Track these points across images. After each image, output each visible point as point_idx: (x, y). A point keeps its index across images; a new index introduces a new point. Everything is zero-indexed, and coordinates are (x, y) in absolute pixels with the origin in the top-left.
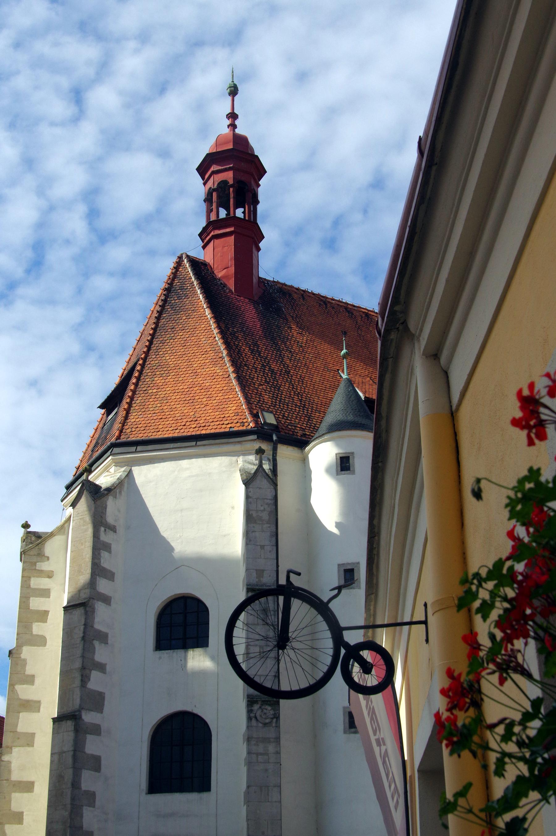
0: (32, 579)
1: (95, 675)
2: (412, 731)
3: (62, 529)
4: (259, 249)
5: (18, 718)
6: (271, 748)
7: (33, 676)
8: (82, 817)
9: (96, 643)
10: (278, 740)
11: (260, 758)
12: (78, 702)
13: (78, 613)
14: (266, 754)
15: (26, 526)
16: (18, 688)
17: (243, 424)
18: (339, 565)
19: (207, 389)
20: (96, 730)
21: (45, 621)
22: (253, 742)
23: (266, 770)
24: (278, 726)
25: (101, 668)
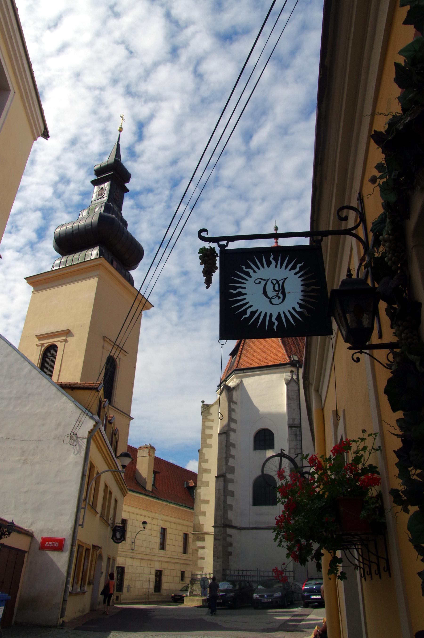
8: (228, 514)
9: (231, 448)
12: (225, 470)
15: (203, 402)
16: (202, 464)
20: (232, 481)
21: (211, 439)
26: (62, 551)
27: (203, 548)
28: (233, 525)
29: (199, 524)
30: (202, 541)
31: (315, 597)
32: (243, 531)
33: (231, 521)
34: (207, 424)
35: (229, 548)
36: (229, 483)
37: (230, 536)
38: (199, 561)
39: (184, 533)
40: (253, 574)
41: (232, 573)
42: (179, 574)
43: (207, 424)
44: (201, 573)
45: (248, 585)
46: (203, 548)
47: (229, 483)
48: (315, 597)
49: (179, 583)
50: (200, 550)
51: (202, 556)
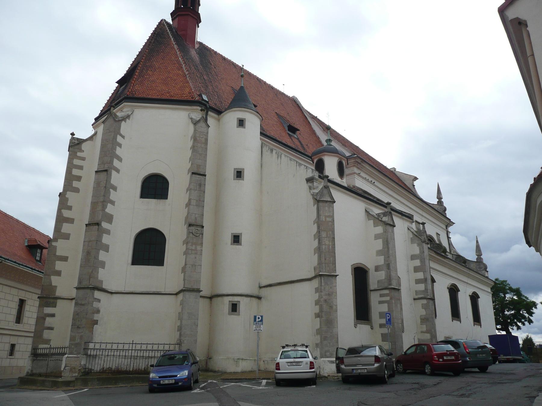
0: (75, 160)
1: (109, 205)
2: (538, 74)
3: (91, 138)
4: (198, 27)
5: (62, 225)
6: (199, 248)
7: (71, 207)
8: (98, 273)
9: (111, 190)
10: (202, 244)
11: (193, 252)
12: (100, 218)
13: (103, 175)
14: (196, 250)
15: (73, 134)
16: (63, 211)
17: (193, 98)
18: (55, 307)
19: (175, 80)
20: (108, 232)
21: (80, 181)
22: (190, 244)
23: (196, 258)
24: (202, 238)
25: (113, 203)
26: (357, 319)
27: (53, 315)
28: (104, 287)
29: (51, 285)
30: (53, 307)
31: (86, 390)
32: (115, 295)
33: (101, 282)
34: (76, 162)
35: (95, 315)
36: (104, 235)
37: (99, 301)
38: (45, 331)
39: (20, 299)
40: (126, 347)
41: (98, 346)
42: (8, 347)
43: (76, 162)
44: (49, 346)
45: (426, 348)
46: (53, 315)
47: (104, 235)
48: (86, 390)
49: (7, 358)
50: (48, 319)
51: (49, 326)
